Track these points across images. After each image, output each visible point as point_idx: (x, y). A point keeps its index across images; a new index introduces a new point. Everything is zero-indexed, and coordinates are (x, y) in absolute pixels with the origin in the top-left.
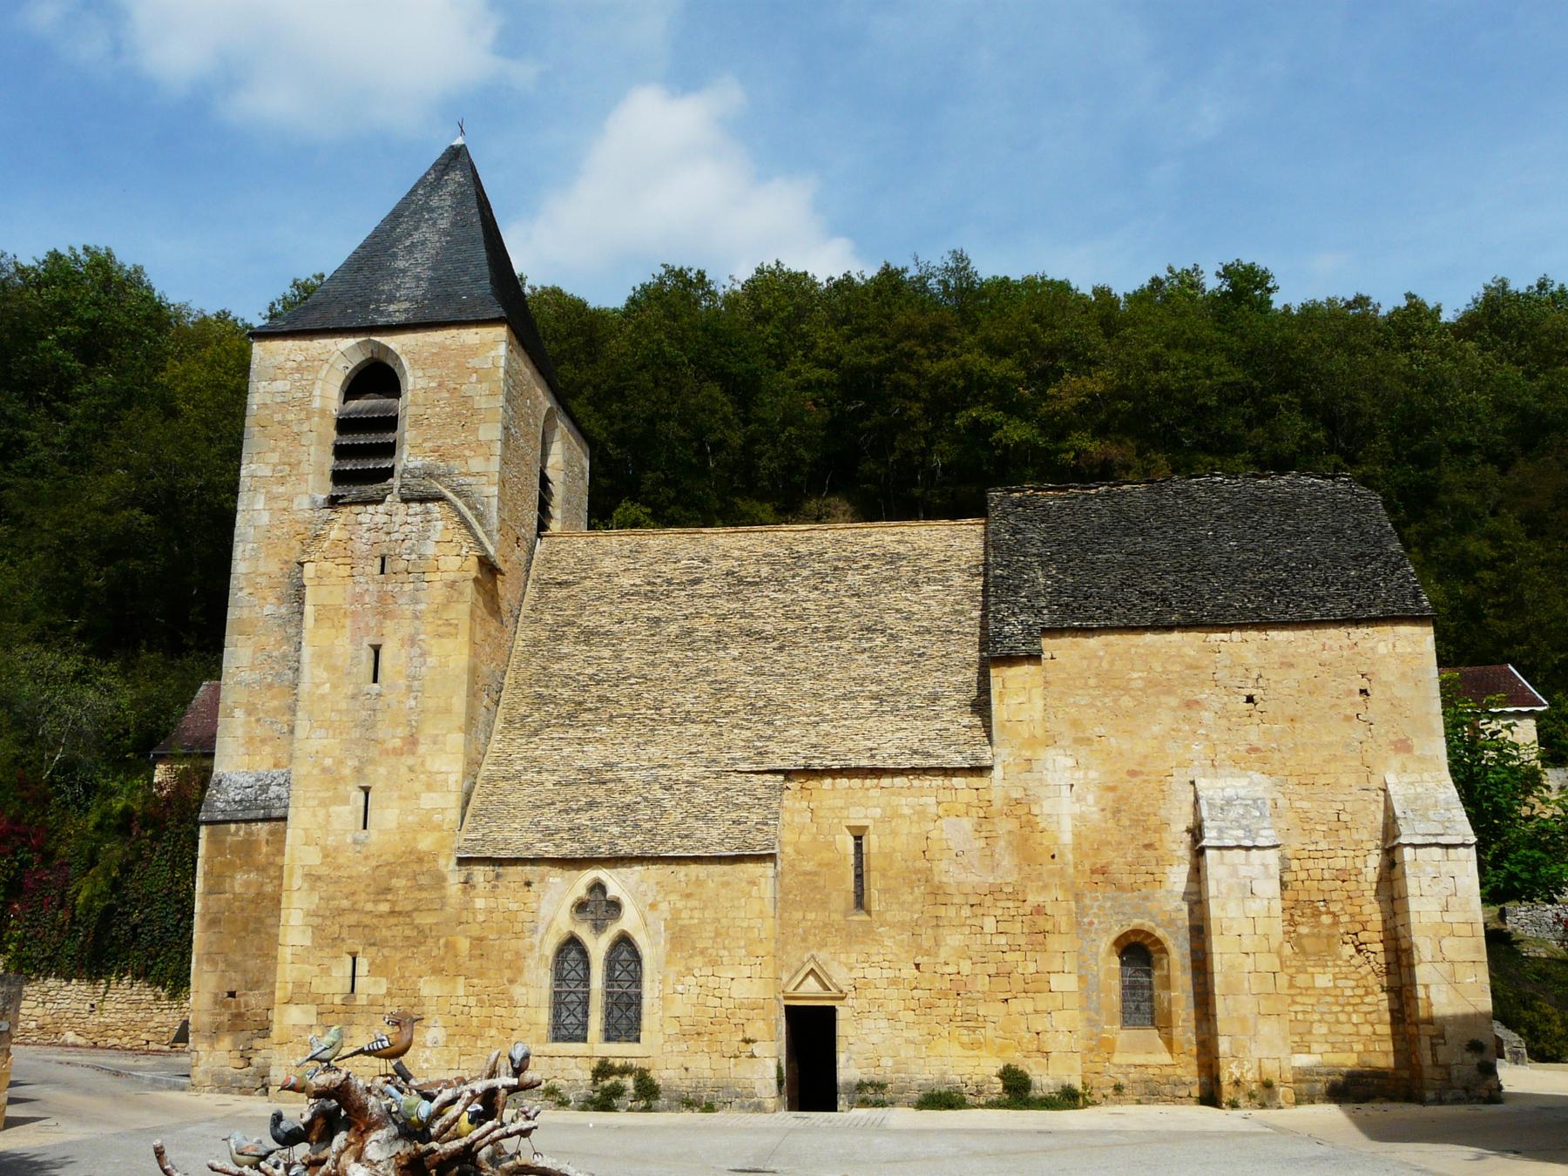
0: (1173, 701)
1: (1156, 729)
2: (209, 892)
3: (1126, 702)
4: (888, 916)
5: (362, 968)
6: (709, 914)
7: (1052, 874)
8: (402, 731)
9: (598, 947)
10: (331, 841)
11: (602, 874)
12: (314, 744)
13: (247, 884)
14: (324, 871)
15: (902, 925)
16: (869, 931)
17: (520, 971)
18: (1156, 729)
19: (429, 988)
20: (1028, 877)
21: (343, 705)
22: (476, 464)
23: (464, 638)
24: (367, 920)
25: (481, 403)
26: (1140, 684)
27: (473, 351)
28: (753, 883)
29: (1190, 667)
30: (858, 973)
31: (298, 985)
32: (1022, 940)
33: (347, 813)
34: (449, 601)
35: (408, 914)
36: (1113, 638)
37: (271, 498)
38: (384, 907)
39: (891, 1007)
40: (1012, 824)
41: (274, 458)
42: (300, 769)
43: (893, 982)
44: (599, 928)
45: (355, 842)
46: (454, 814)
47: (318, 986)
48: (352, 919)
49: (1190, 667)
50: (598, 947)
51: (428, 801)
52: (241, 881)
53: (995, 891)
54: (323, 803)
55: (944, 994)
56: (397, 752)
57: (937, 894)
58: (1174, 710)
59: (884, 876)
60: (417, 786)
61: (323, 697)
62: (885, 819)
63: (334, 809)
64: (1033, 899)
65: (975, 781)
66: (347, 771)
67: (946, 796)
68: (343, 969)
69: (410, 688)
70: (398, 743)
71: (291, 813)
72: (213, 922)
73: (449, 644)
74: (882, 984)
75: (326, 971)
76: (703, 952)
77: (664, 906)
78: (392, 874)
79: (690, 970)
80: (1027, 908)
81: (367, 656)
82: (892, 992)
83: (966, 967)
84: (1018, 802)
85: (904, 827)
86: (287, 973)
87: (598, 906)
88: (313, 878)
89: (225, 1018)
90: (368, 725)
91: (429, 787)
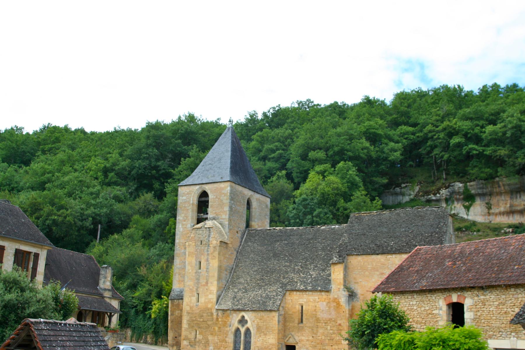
0: (378, 273)
1: (373, 280)
2: (171, 315)
3: (367, 273)
4: (307, 325)
5: (198, 333)
6: (265, 323)
7: (343, 316)
8: (205, 281)
9: (243, 330)
10: (192, 305)
11: (243, 313)
12: (188, 283)
13: (178, 313)
14: (190, 311)
15: (309, 327)
16: (303, 327)
17: (227, 335)
18: (373, 280)
19: (210, 338)
20: (338, 317)
21: (194, 275)
22: (224, 217)
23: (217, 260)
24: (198, 322)
25: (225, 201)
26: (370, 269)
27: (222, 189)
28: (274, 317)
29: (382, 264)
30: (300, 338)
31: (186, 336)
32: (336, 332)
33: (194, 299)
34: (214, 251)
35: (206, 321)
36: (364, 257)
37: (183, 225)
38: (202, 320)
39: (307, 346)
40: (335, 304)
41: (183, 215)
42: (186, 289)
43: (308, 340)
44: (243, 326)
45: (196, 305)
46: (215, 300)
47: (189, 336)
48: (196, 322)
49: (382, 264)
50: (243, 330)
51: (210, 296)
52: (177, 313)
53: (330, 320)
54: (190, 297)
55: (318, 344)
56: (204, 285)
57: (318, 320)
58: (378, 275)
59: (306, 315)
60: (208, 293)
61: (190, 273)
62: (306, 302)
63: (192, 298)
64: (339, 322)
65: (327, 294)
66: (194, 289)
67: (321, 297)
68: (193, 333)
69: (207, 271)
70: (204, 283)
71: (184, 298)
72: (172, 322)
73: (214, 261)
74: (305, 341)
75: (191, 333)
76: (263, 332)
77: (256, 321)
78: (203, 313)
79: (260, 336)
80: (338, 324)
81: (198, 263)
82: (307, 342)
83: (323, 337)
84: (336, 298)
85: (311, 304)
86: (184, 333)
87: (243, 321)
88: (188, 313)
89: (174, 342)
90: (198, 279)
91: (210, 294)
